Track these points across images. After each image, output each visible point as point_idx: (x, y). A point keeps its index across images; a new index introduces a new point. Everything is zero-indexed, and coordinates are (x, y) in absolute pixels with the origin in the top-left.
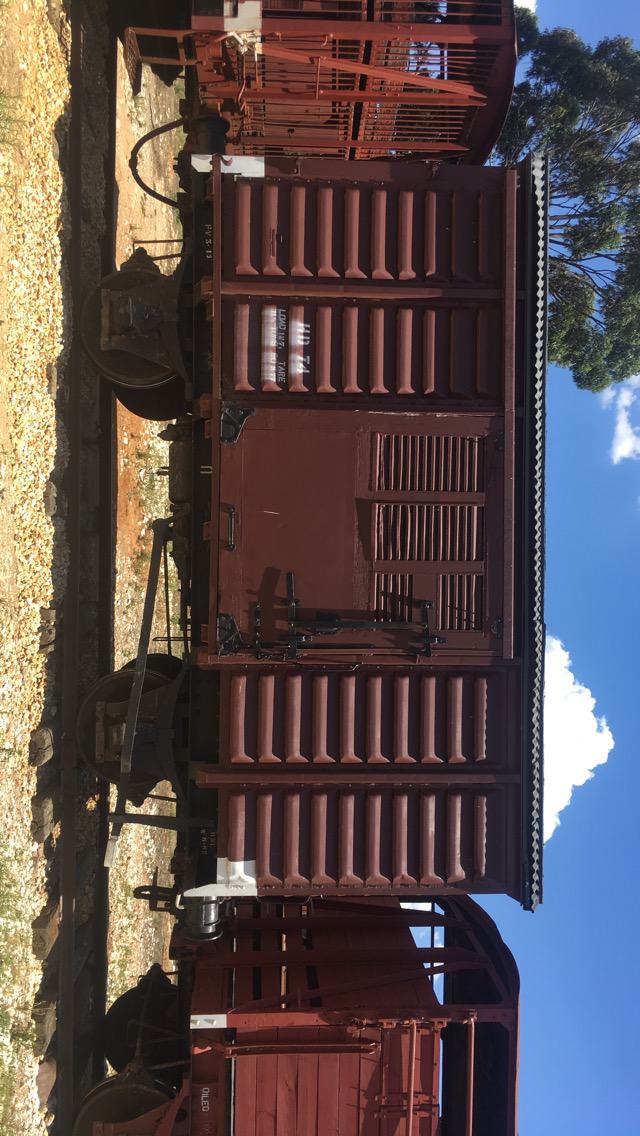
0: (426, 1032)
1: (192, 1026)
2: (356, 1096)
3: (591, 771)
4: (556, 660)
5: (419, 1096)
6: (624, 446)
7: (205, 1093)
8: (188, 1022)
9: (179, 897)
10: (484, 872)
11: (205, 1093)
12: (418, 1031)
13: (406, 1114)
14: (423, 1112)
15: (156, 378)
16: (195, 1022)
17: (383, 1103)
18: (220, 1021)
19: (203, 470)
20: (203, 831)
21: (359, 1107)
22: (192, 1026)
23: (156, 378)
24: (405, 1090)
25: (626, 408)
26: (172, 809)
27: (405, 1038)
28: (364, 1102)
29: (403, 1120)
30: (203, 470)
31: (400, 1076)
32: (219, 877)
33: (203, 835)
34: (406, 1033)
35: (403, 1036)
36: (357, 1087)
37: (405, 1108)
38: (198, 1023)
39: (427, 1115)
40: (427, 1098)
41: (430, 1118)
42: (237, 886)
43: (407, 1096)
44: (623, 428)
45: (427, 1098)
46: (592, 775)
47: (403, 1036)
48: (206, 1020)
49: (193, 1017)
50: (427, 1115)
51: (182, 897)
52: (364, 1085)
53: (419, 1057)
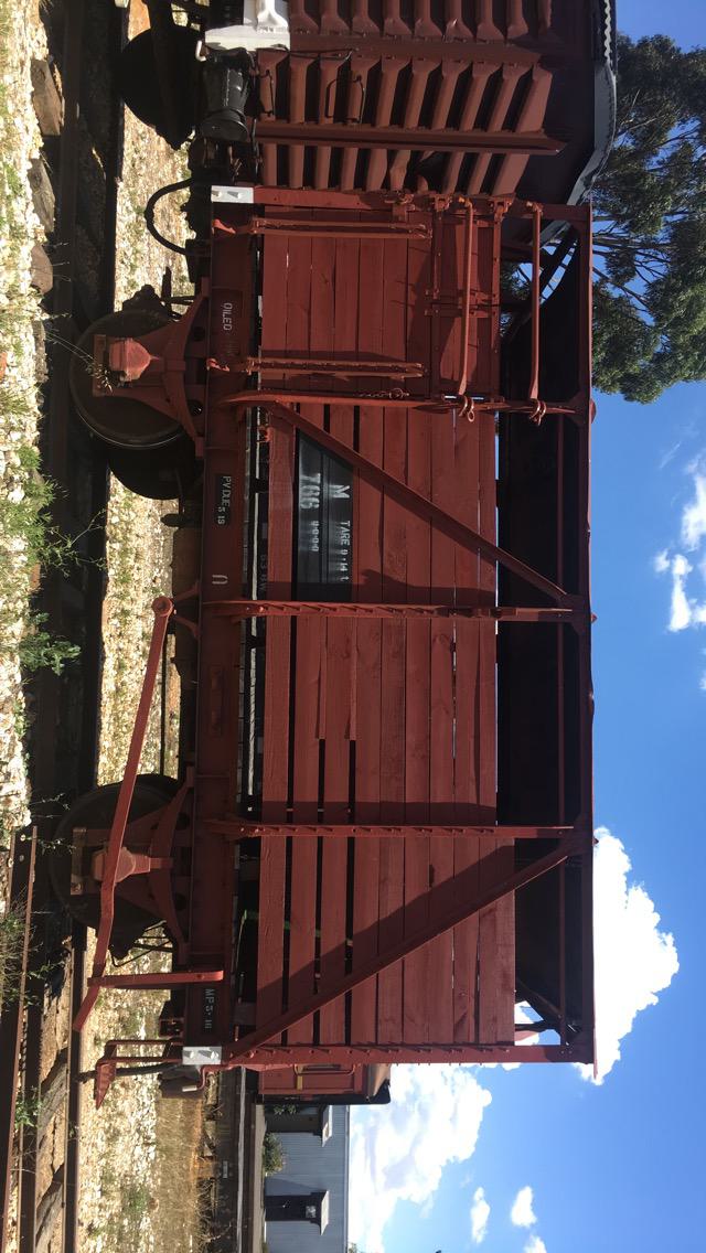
0: (485, 224)
1: (214, 199)
2: (404, 290)
3: (656, 994)
4: (609, 859)
5: (475, 313)
6: (681, 615)
7: (227, 309)
8: (209, 192)
9: (200, 44)
10: (549, 24)
11: (227, 309)
12: (474, 222)
13: (461, 314)
14: (481, 312)
15: (160, 434)
16: (216, 194)
17: (435, 298)
18: (245, 195)
19: (216, 579)
20: (228, 8)
21: (407, 305)
22: (214, 199)
23: (160, 434)
24: (460, 287)
25: (681, 577)
26: (166, 964)
27: (459, 229)
28: (412, 297)
29: (458, 320)
30: (216, 579)
31: (455, 275)
32: (246, 20)
33: (227, 12)
34: (462, 223)
35: (458, 227)
36: (403, 281)
37: (460, 307)
38: (220, 194)
39: (486, 315)
40: (486, 297)
41: (490, 319)
42: (266, 29)
43: (462, 293)
44: (679, 599)
45: (486, 297)
46: (655, 1000)
47: (458, 227)
48: (229, 193)
49: (214, 188)
50: (486, 315)
51: (204, 44)
52: (412, 280)
53: (476, 252)
